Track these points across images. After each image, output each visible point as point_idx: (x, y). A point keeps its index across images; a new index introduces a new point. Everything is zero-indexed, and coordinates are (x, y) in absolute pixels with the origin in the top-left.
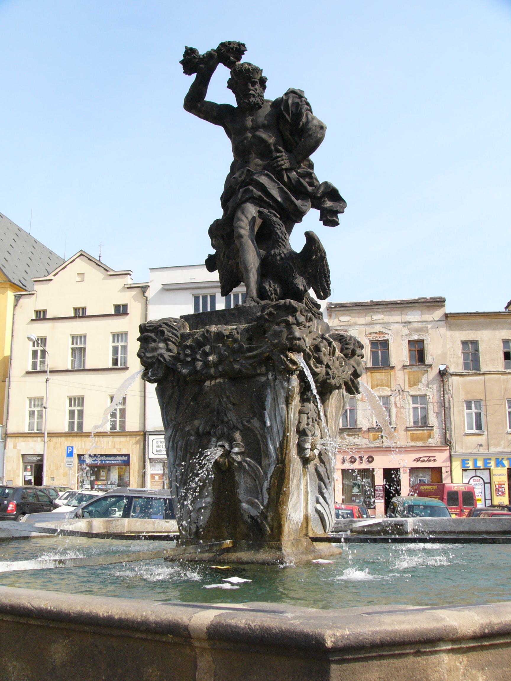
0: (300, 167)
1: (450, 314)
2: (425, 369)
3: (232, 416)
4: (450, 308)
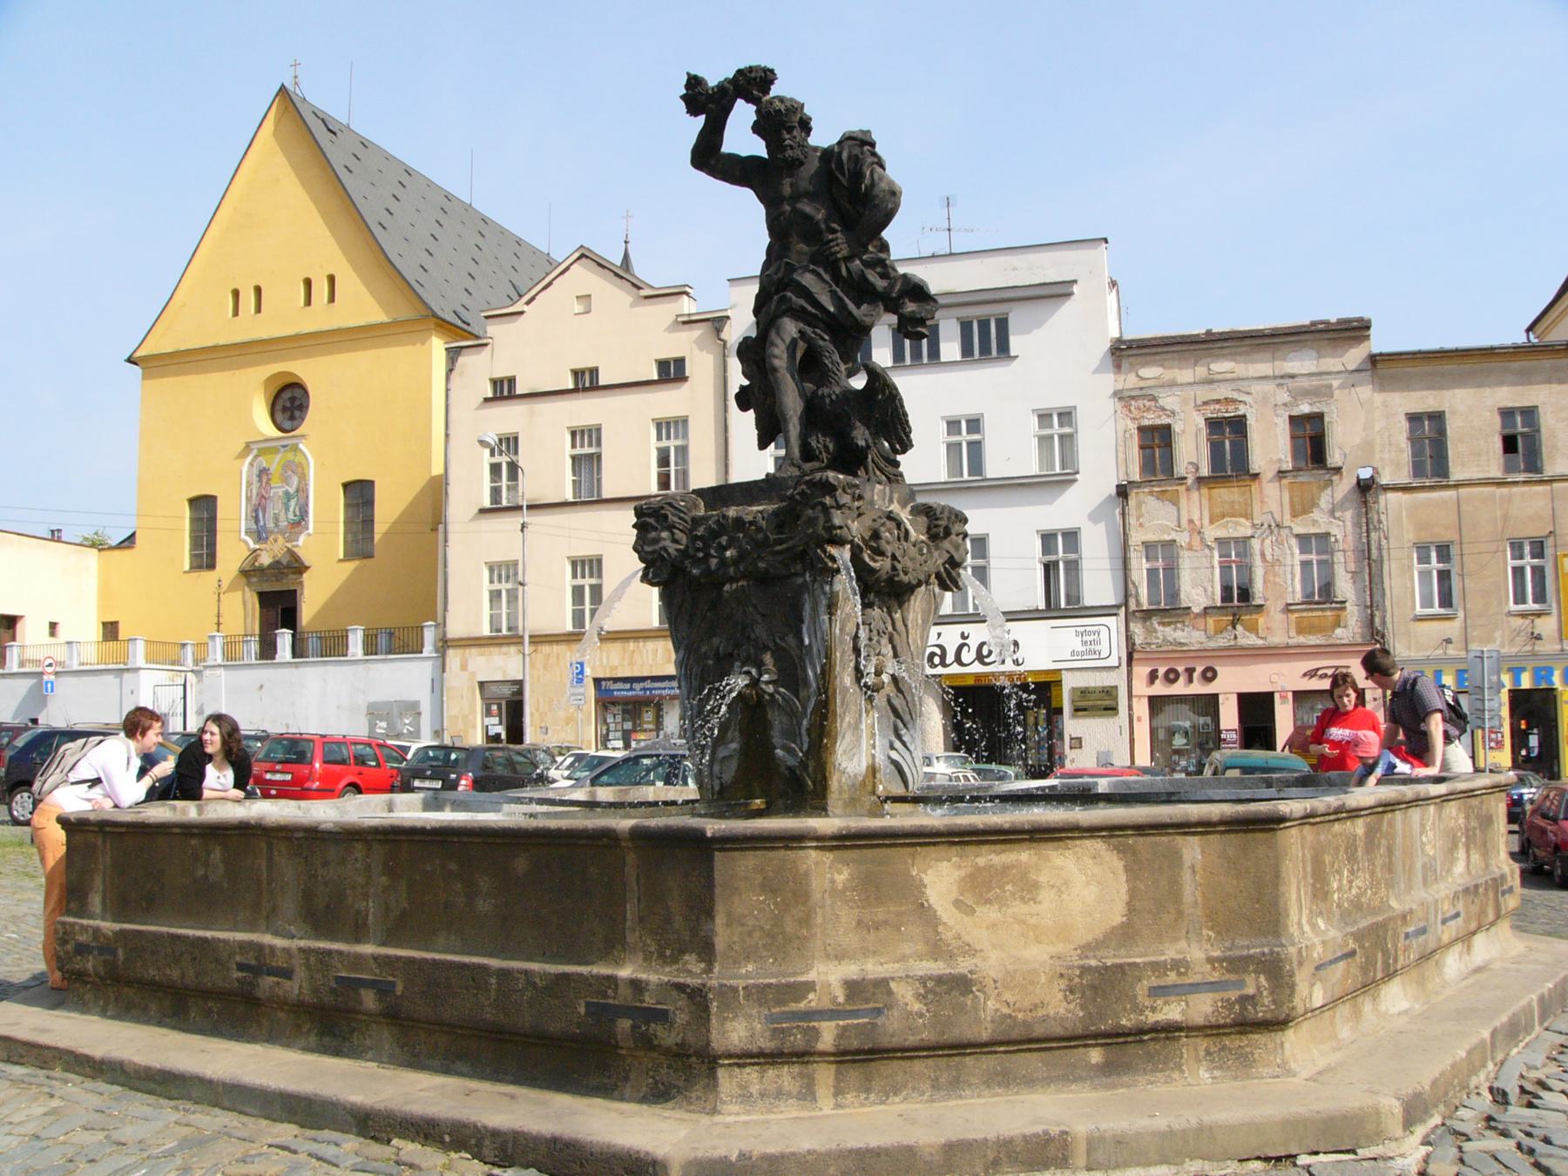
0: (866, 251)
3: (760, 632)
4: (1381, 341)
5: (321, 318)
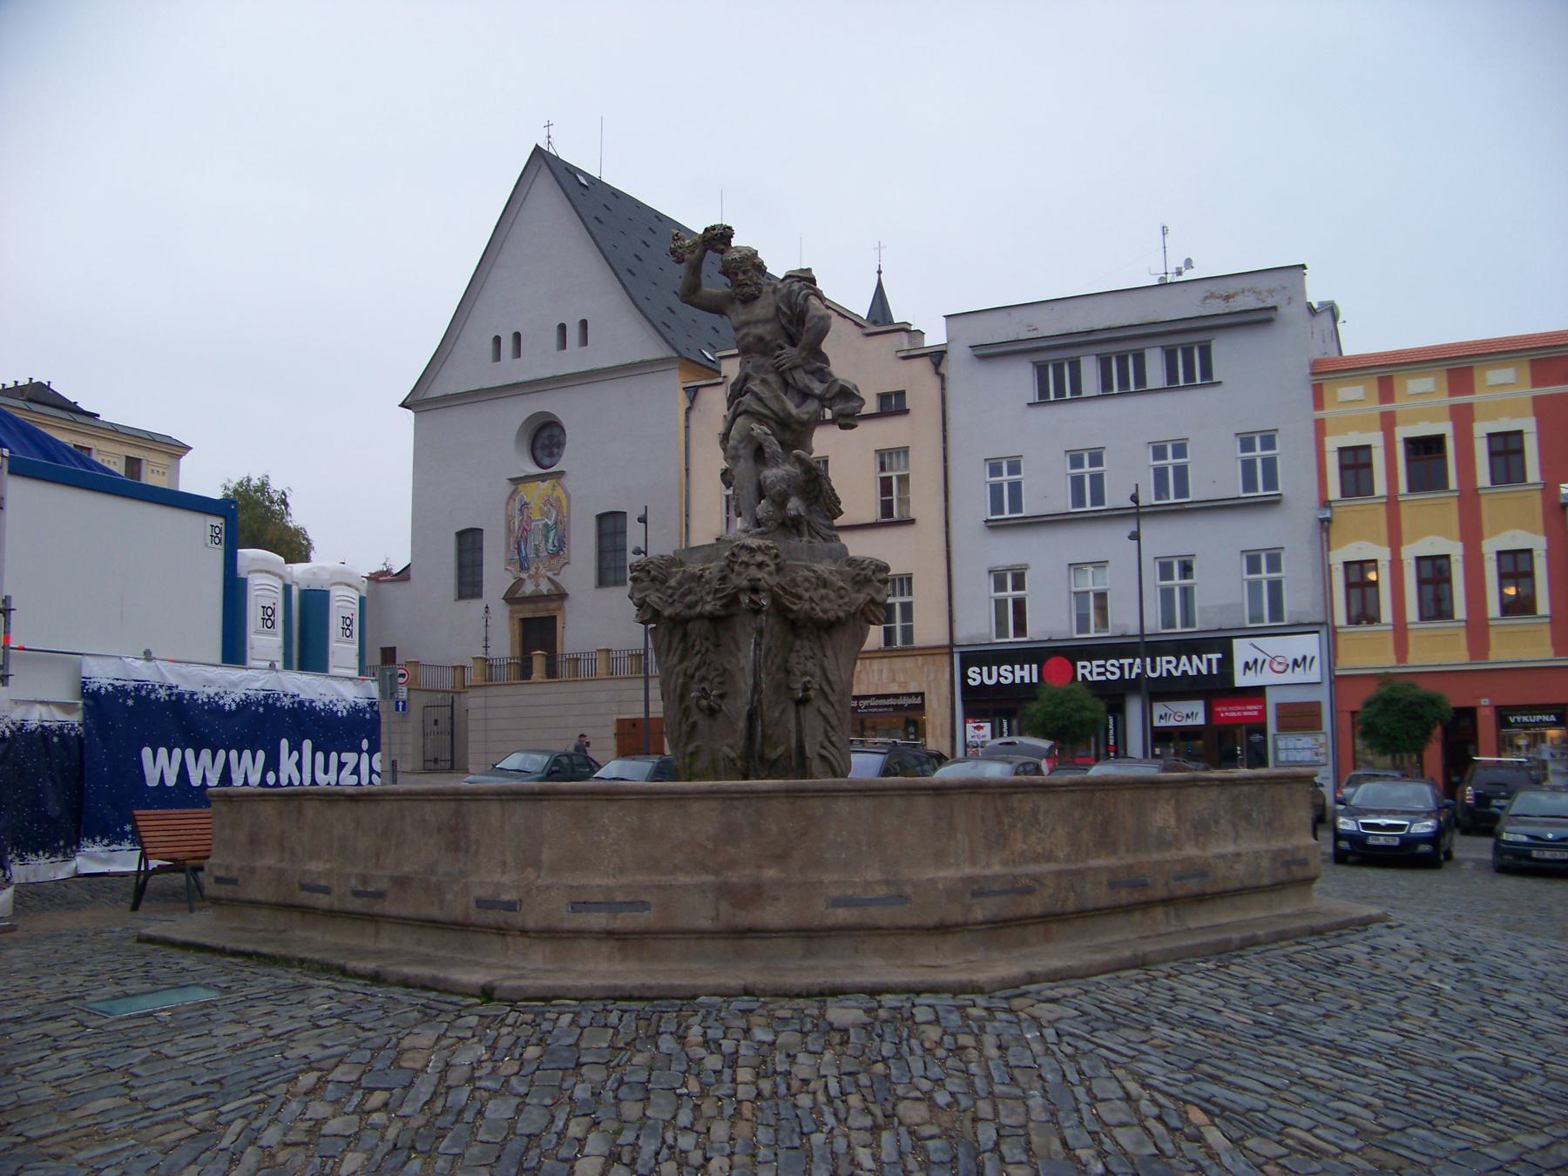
5: (575, 360)
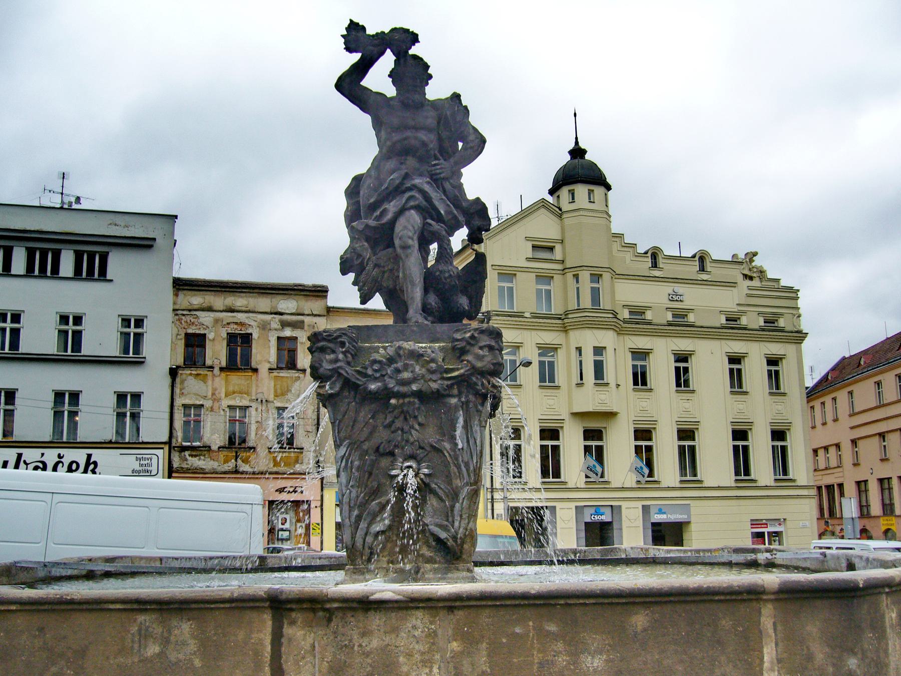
1: (333, 308)
2: (297, 375)
